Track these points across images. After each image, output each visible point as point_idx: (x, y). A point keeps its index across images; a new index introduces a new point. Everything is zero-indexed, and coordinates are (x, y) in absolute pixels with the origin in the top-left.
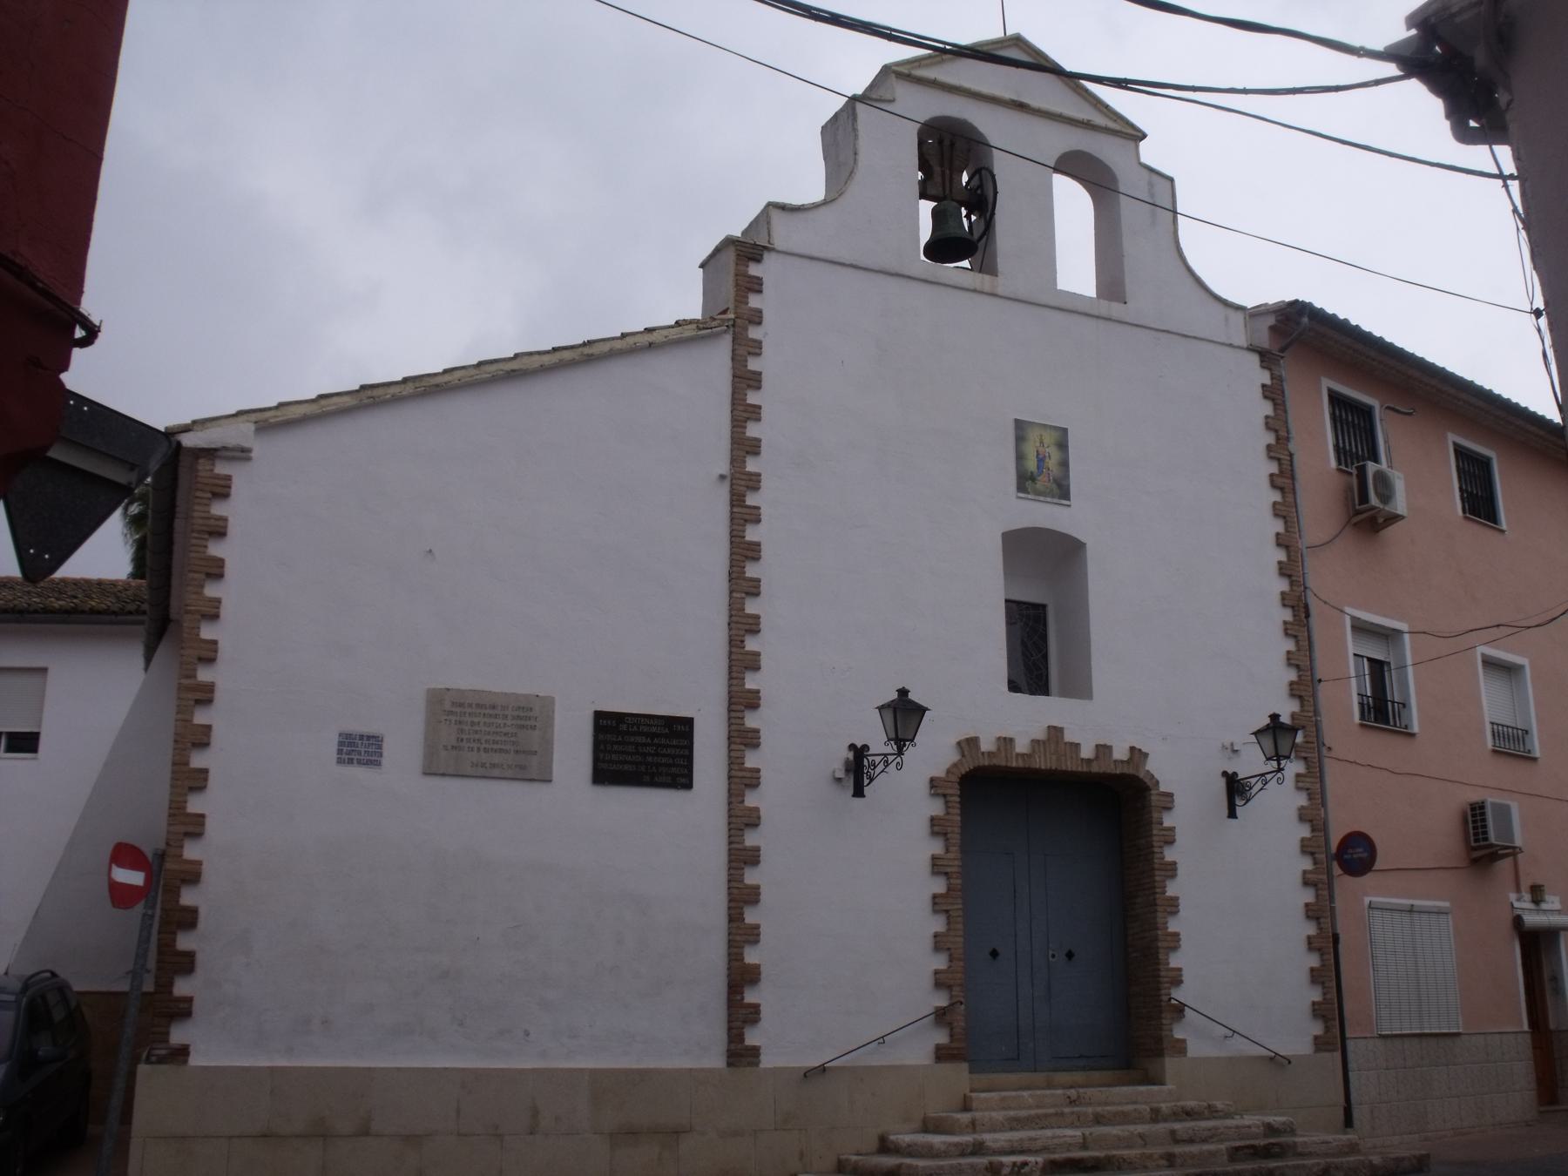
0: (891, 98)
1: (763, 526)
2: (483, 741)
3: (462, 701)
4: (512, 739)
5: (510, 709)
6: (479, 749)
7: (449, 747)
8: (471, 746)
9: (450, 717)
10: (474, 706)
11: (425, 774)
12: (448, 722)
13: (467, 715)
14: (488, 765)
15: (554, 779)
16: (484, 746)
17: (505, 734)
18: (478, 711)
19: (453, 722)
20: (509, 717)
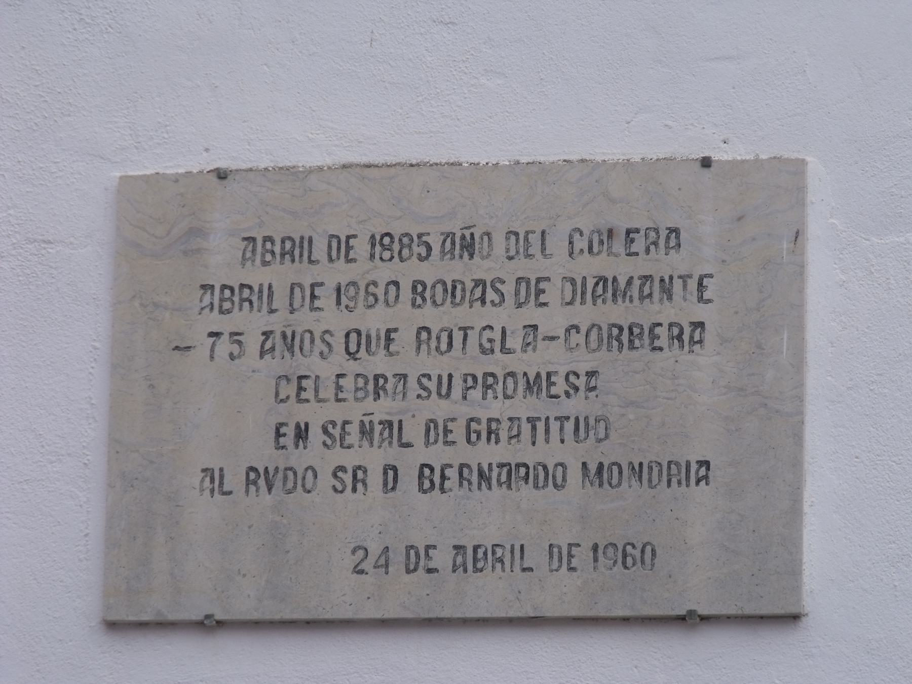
0: (224, 176)
1: (398, 334)
2: (414, 432)
3: (297, 230)
4: (574, 406)
5: (557, 244)
6: (391, 473)
7: (235, 480)
8: (350, 459)
9: (239, 319)
10: (361, 248)
11: (113, 626)
12: (224, 347)
13: (326, 299)
14: (442, 558)
15: (809, 604)
16: (421, 454)
17: (533, 385)
18: (384, 273)
19: (253, 343)
20: (553, 293)
